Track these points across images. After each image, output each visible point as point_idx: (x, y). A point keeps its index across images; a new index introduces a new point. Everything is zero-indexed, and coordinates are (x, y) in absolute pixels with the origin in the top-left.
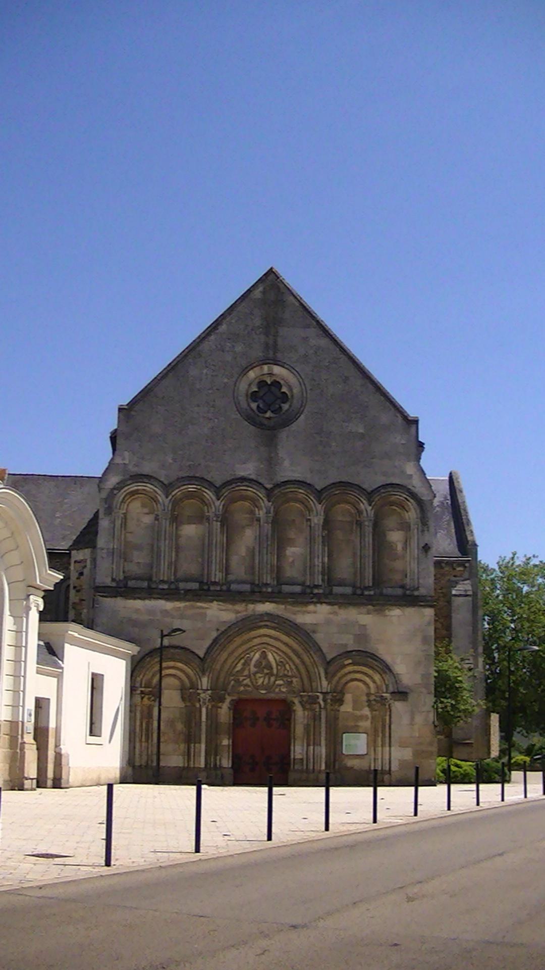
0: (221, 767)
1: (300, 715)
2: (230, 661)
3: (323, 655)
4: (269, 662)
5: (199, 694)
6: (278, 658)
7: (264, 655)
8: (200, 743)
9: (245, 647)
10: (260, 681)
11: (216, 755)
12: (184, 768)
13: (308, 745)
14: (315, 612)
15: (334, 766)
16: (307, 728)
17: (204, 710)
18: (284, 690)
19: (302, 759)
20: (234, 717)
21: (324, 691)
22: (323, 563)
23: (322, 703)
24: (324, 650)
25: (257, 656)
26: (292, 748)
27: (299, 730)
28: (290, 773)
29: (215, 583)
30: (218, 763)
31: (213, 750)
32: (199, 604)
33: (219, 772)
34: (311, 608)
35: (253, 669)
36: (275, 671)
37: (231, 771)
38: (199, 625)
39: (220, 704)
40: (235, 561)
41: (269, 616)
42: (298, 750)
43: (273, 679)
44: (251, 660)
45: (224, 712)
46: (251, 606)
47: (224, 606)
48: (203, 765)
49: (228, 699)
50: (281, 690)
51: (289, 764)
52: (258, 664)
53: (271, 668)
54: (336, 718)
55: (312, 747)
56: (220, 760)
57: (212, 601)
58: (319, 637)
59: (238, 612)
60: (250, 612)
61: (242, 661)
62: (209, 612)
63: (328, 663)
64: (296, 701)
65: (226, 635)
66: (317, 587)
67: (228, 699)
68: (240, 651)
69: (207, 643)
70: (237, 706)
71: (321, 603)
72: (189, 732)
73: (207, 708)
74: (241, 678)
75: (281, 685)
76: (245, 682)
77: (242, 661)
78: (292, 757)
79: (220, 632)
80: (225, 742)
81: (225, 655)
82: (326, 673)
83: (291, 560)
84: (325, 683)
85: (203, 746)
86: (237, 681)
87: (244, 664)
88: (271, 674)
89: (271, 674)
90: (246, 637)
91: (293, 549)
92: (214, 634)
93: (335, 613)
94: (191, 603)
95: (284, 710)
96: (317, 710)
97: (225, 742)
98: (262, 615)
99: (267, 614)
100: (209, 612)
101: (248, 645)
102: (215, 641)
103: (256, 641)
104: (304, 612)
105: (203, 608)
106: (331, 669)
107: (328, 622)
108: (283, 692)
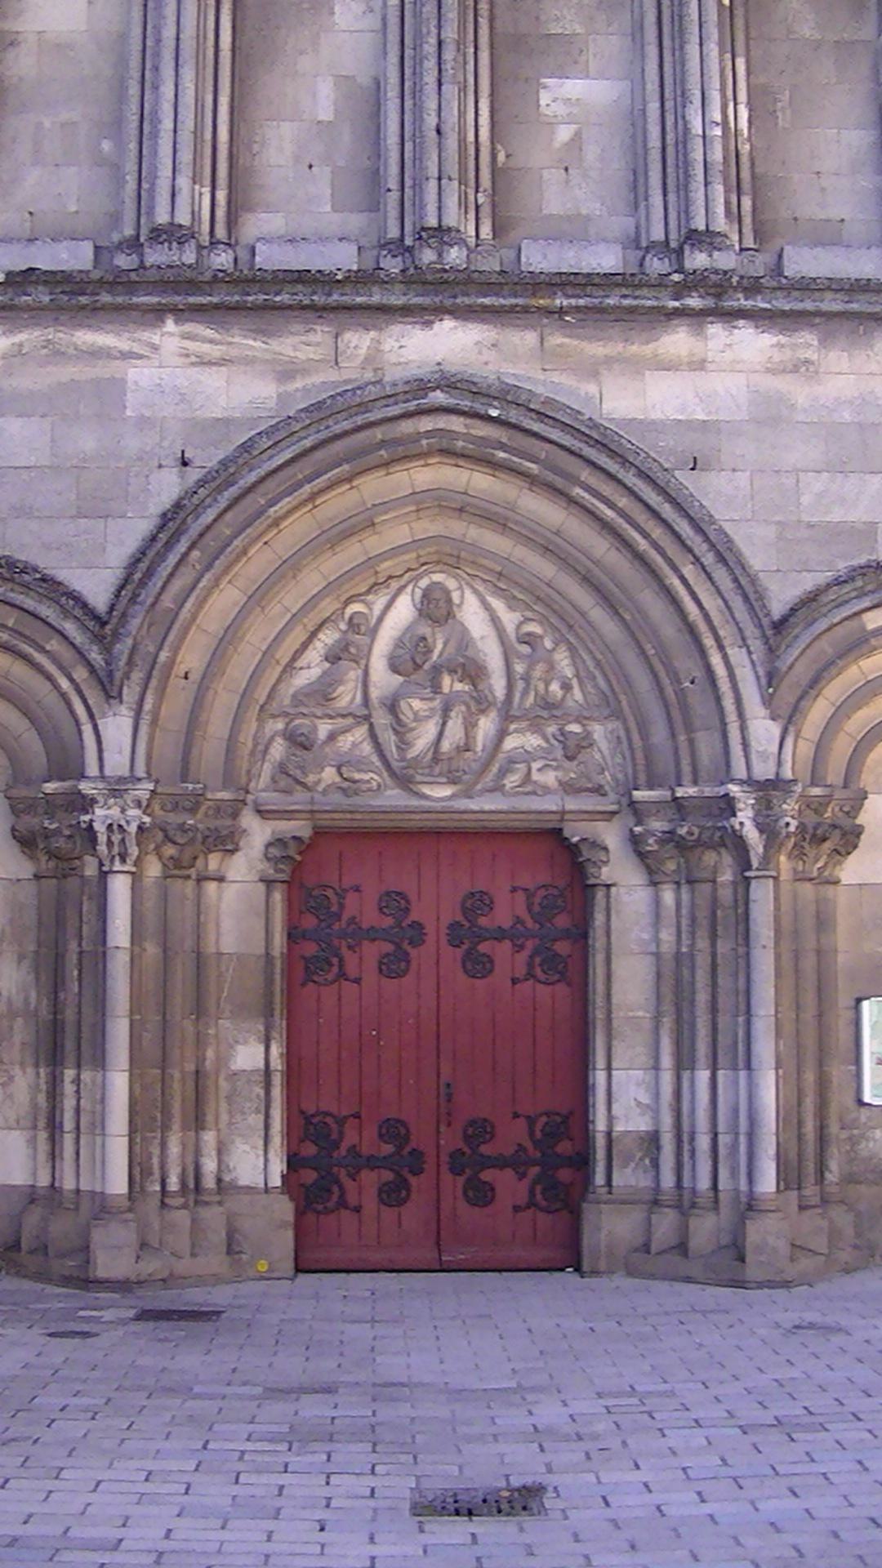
0: (223, 1186)
1: (634, 910)
2: (257, 636)
3: (751, 593)
4: (464, 640)
5: (87, 804)
6: (509, 619)
7: (436, 609)
8: (100, 1061)
9: (333, 564)
10: (423, 739)
11: (197, 1121)
12: (32, 1196)
13: (684, 1062)
14: (699, 365)
15: (821, 1169)
16: (675, 985)
17: (120, 888)
18: (550, 778)
19: (653, 1138)
20: (294, 935)
21: (764, 770)
22: (729, 133)
23: (751, 834)
24: (757, 560)
25: (403, 611)
26: (600, 1077)
27: (628, 980)
28: (589, 1211)
29: (171, 234)
30: (210, 1165)
31: (176, 1097)
32: (87, 337)
33: (213, 1216)
34: (677, 341)
35: (382, 679)
36: (498, 685)
37: (285, 1208)
38: (87, 441)
39: (214, 862)
40: (279, 148)
41: (464, 392)
42: (628, 1095)
43: (486, 726)
44: (374, 632)
45: (238, 905)
46: (358, 341)
47: (205, 338)
48: (118, 1183)
49: (257, 833)
50: (531, 781)
51: (582, 1161)
52: (411, 659)
53: (473, 672)
54: (823, 921)
55: (703, 1076)
56: (221, 1150)
57: (157, 314)
58: (720, 494)
59: (286, 372)
60: (351, 371)
61: (328, 637)
62: (138, 375)
63: (780, 625)
64: (611, 836)
65: (224, 498)
66: (706, 239)
67: (257, 833)
68: (312, 580)
69: (130, 533)
70: (311, 870)
71: (730, 316)
72: (56, 1008)
73: (136, 877)
74: (324, 729)
75: (528, 757)
76: (346, 742)
77: (328, 637)
78: (601, 1125)
79: (194, 475)
80: (248, 1056)
81: (226, 599)
82: (771, 678)
83: (564, 133)
84: (764, 730)
85: (119, 1083)
86: (300, 742)
87: (333, 657)
88: (481, 703)
89: (481, 703)
90: (338, 503)
91: (574, 87)
92: (167, 487)
93: (798, 367)
94: (50, 333)
95: (561, 864)
96: (726, 877)
97: (248, 1056)
98: (421, 387)
99: (449, 382)
100: (138, 375)
101: (351, 553)
102: (173, 520)
103: (396, 533)
104: (637, 367)
105: (97, 354)
106: (797, 657)
107: (770, 415)
108: (547, 790)
